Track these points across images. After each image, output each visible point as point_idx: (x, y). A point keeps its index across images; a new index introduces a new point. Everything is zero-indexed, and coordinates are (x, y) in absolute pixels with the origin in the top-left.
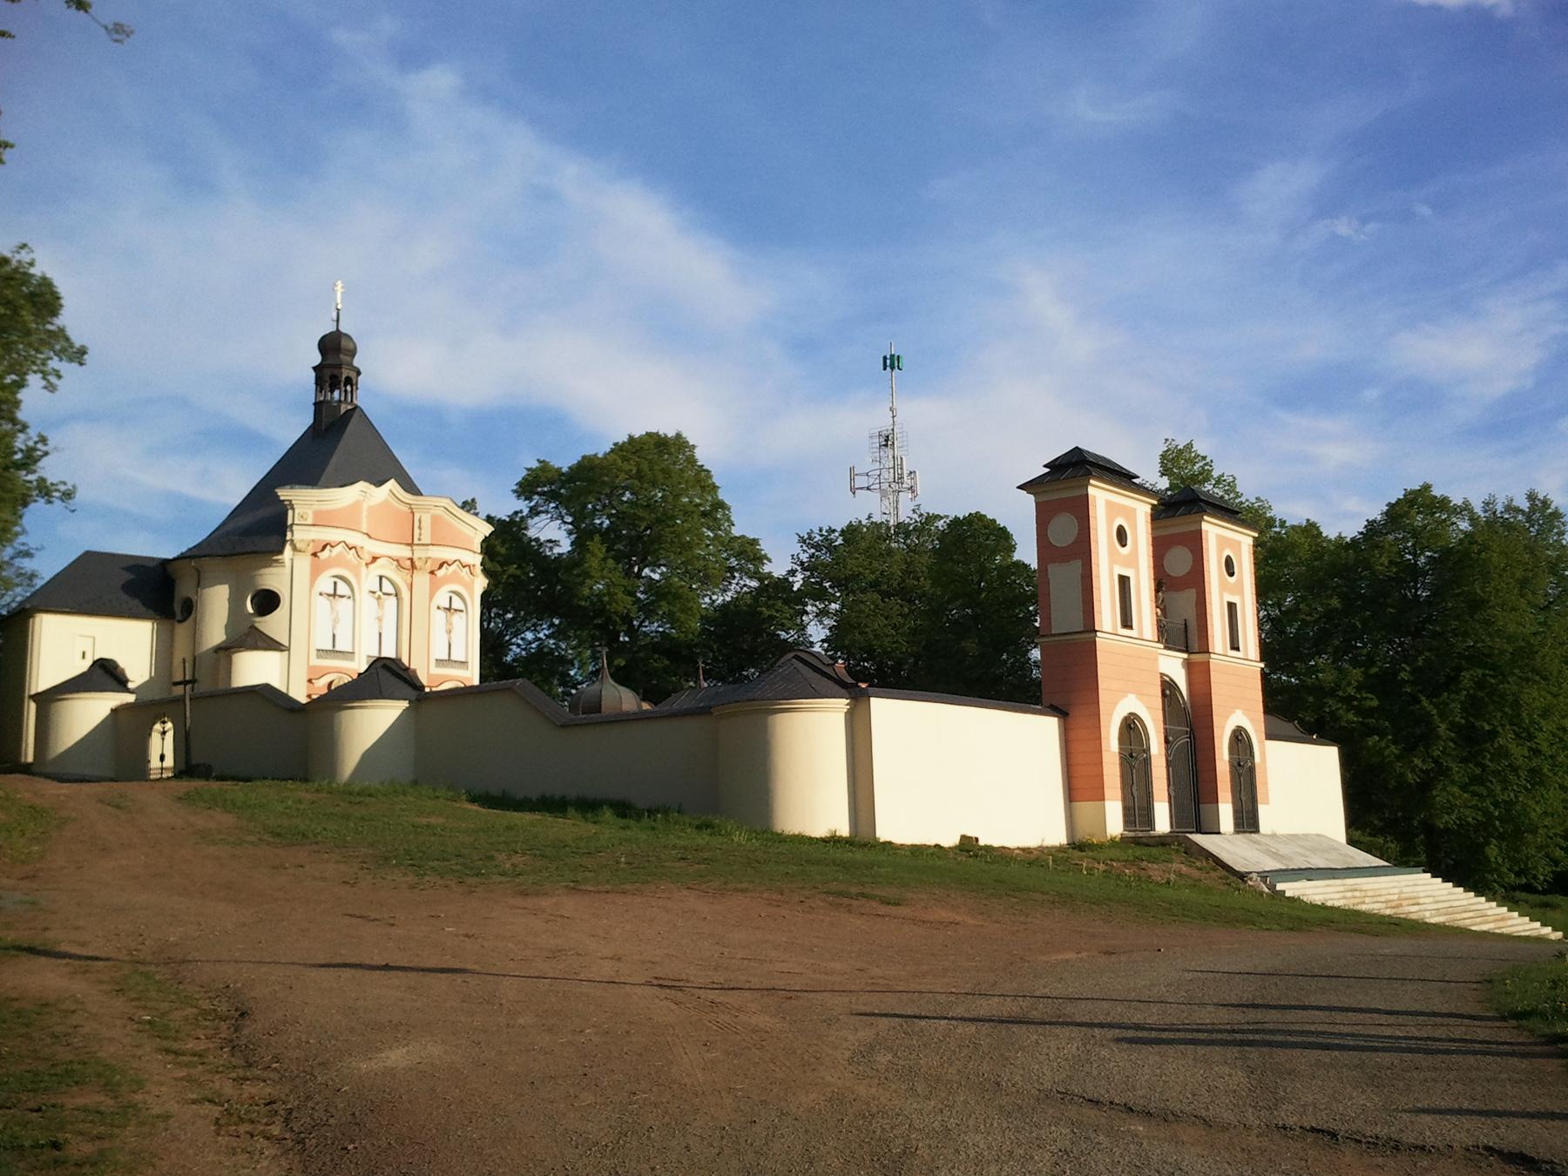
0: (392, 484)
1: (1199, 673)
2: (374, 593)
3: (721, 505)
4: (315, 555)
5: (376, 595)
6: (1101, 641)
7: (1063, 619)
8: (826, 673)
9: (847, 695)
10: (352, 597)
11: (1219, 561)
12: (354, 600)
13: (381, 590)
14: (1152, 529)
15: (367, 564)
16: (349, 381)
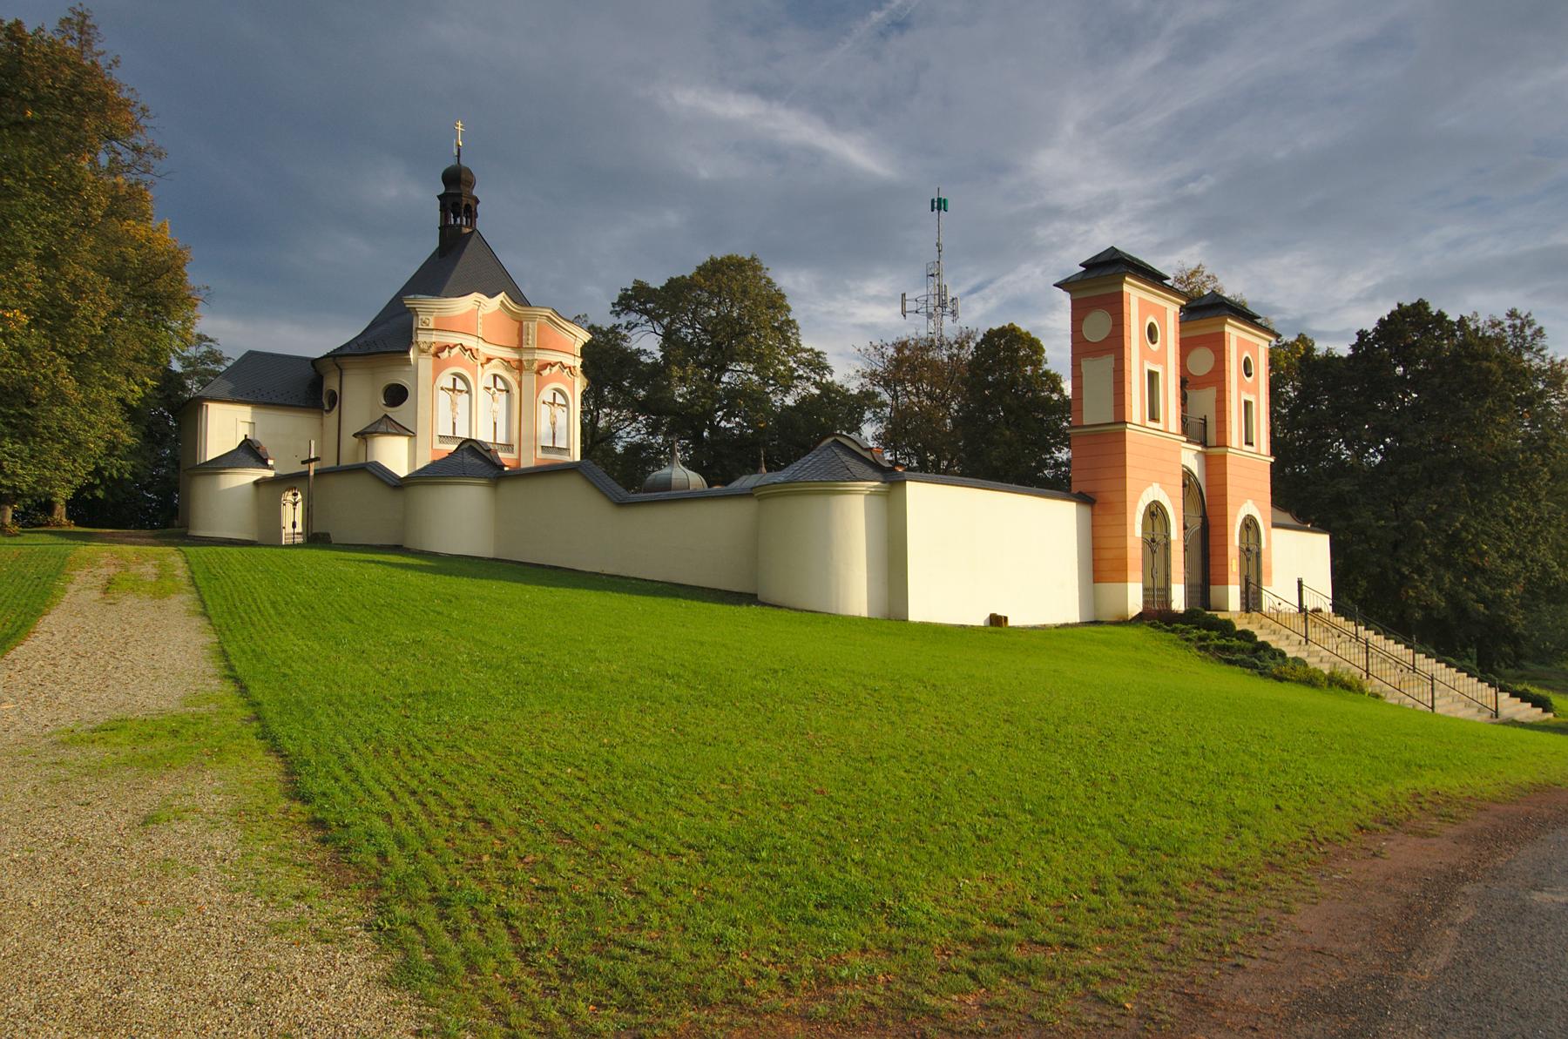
0: (502, 296)
1: (1215, 463)
2: (489, 389)
3: (790, 323)
4: (436, 355)
5: (491, 392)
6: (1131, 433)
7: (1094, 412)
8: (864, 457)
9: (881, 479)
10: (469, 392)
11: (1239, 362)
12: (471, 395)
13: (495, 386)
14: (1181, 331)
15: (481, 364)
16: (468, 207)
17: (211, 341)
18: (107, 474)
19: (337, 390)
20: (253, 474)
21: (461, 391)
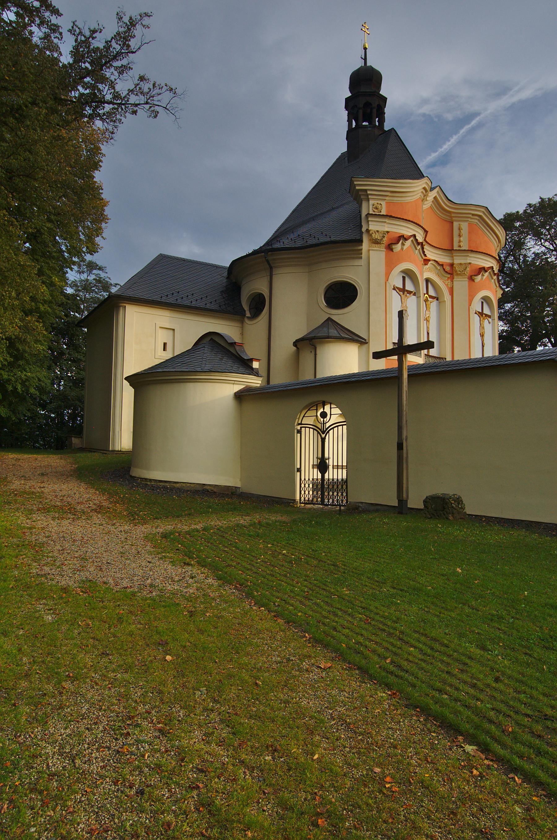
17: (100, 269)
18: (10, 388)
19: (265, 292)
20: (234, 382)
21: (410, 292)
